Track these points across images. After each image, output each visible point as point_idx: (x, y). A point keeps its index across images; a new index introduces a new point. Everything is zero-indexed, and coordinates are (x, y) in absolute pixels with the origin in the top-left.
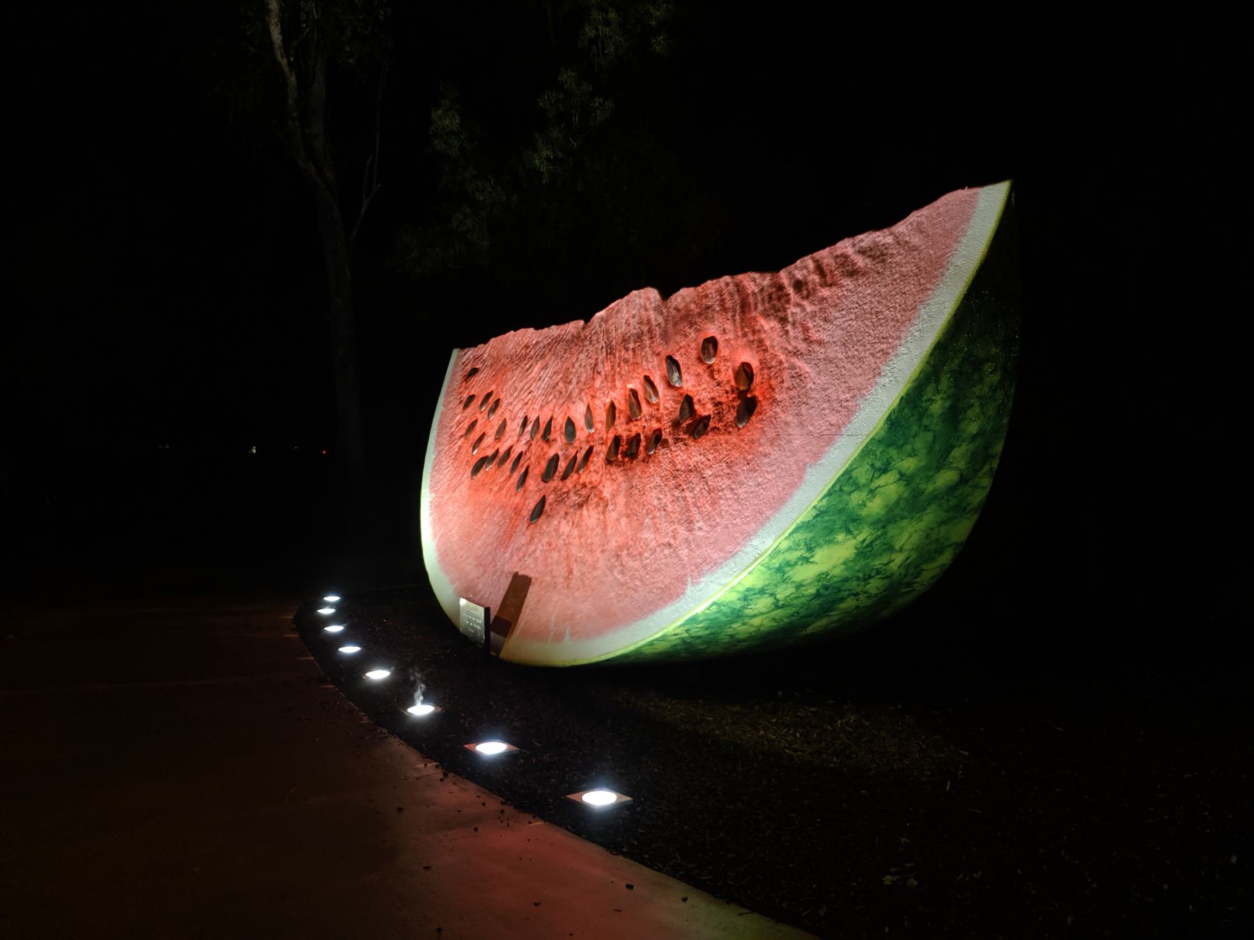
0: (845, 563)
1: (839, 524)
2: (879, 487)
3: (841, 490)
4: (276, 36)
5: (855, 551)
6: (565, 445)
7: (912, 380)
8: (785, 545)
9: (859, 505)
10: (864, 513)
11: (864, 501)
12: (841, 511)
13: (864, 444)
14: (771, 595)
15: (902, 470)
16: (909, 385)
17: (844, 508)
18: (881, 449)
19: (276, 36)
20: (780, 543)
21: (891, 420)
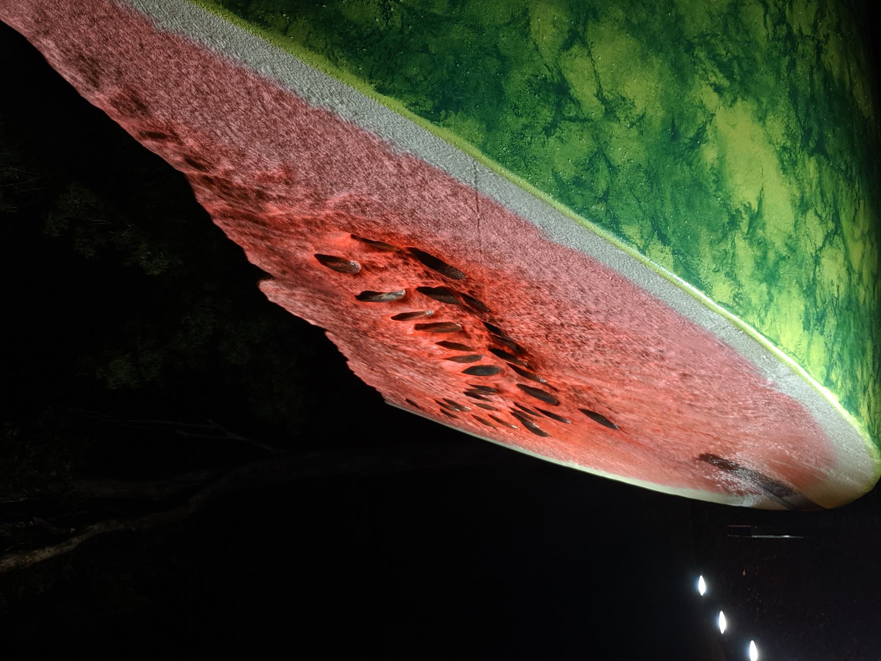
0: (762, 119)
1: (683, 173)
2: (599, 95)
3: (604, 198)
4: (46, 553)
5: (739, 103)
6: (504, 377)
7: (334, 69)
8: (723, 289)
9: (641, 133)
10: (657, 114)
11: (632, 124)
12: (653, 178)
13: (498, 167)
14: (817, 261)
15: (560, 41)
16: (347, 75)
17: (646, 172)
18: (509, 119)
19: (46, 553)
20: (719, 303)
21: (437, 110)
